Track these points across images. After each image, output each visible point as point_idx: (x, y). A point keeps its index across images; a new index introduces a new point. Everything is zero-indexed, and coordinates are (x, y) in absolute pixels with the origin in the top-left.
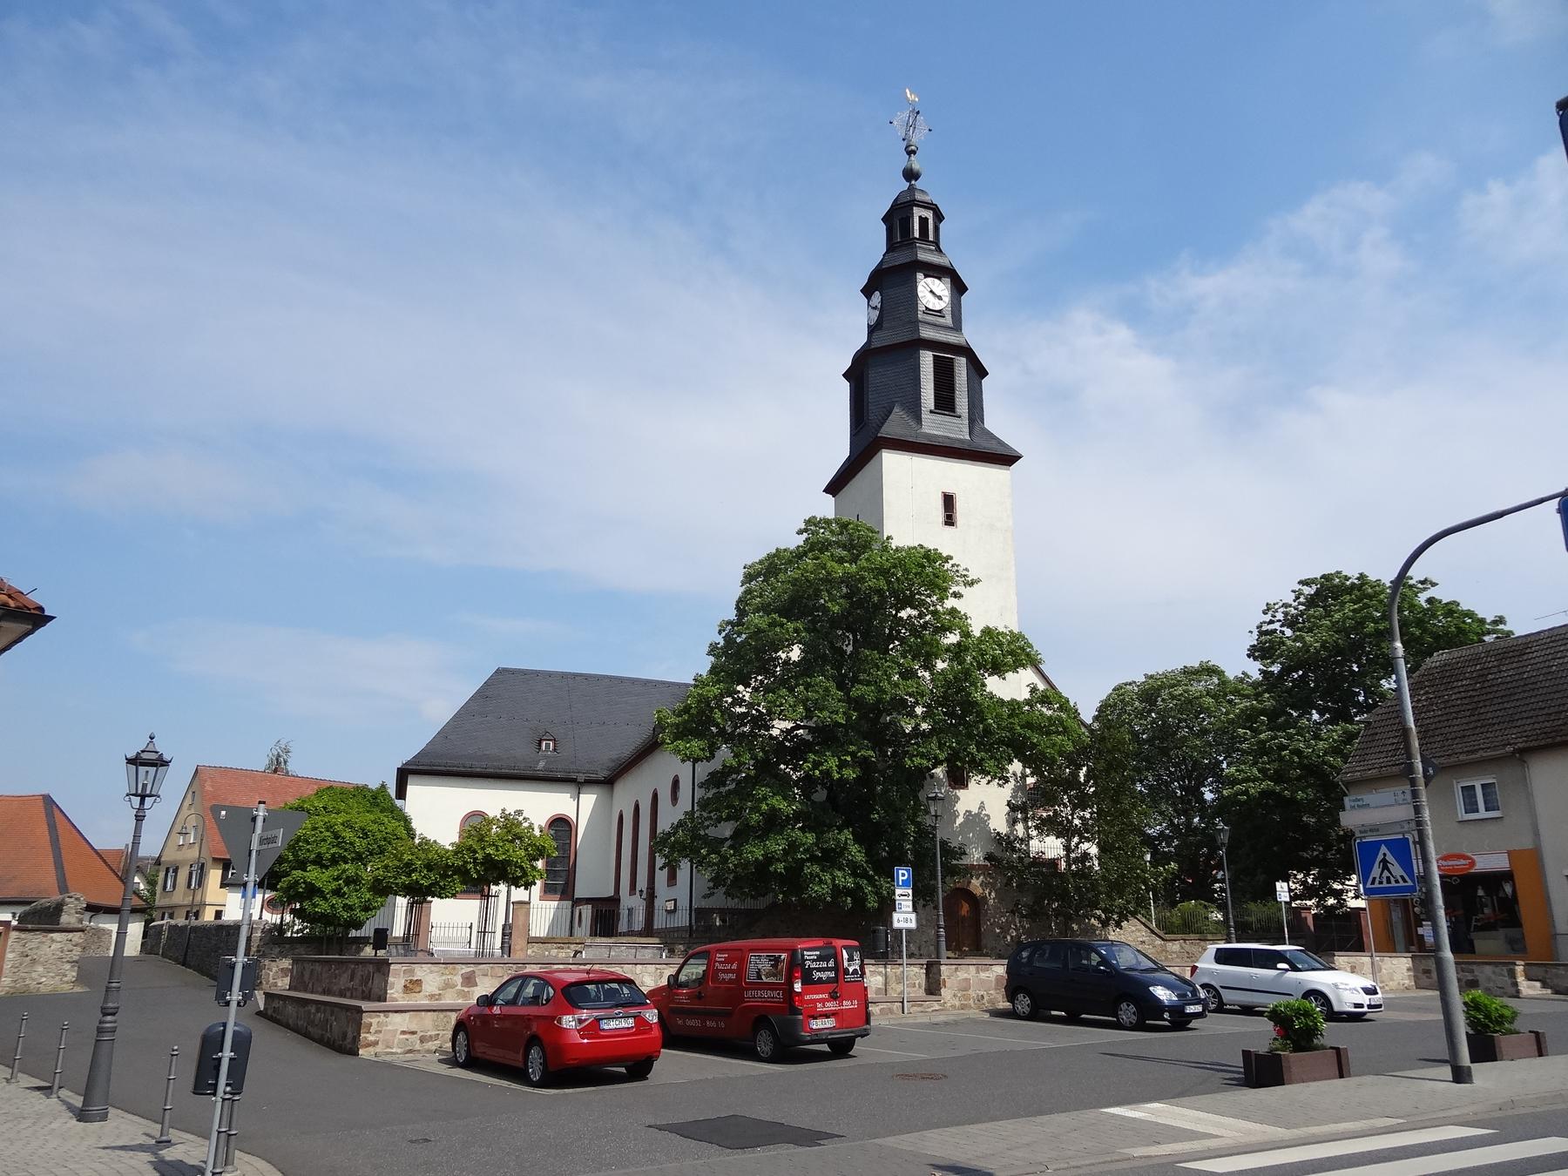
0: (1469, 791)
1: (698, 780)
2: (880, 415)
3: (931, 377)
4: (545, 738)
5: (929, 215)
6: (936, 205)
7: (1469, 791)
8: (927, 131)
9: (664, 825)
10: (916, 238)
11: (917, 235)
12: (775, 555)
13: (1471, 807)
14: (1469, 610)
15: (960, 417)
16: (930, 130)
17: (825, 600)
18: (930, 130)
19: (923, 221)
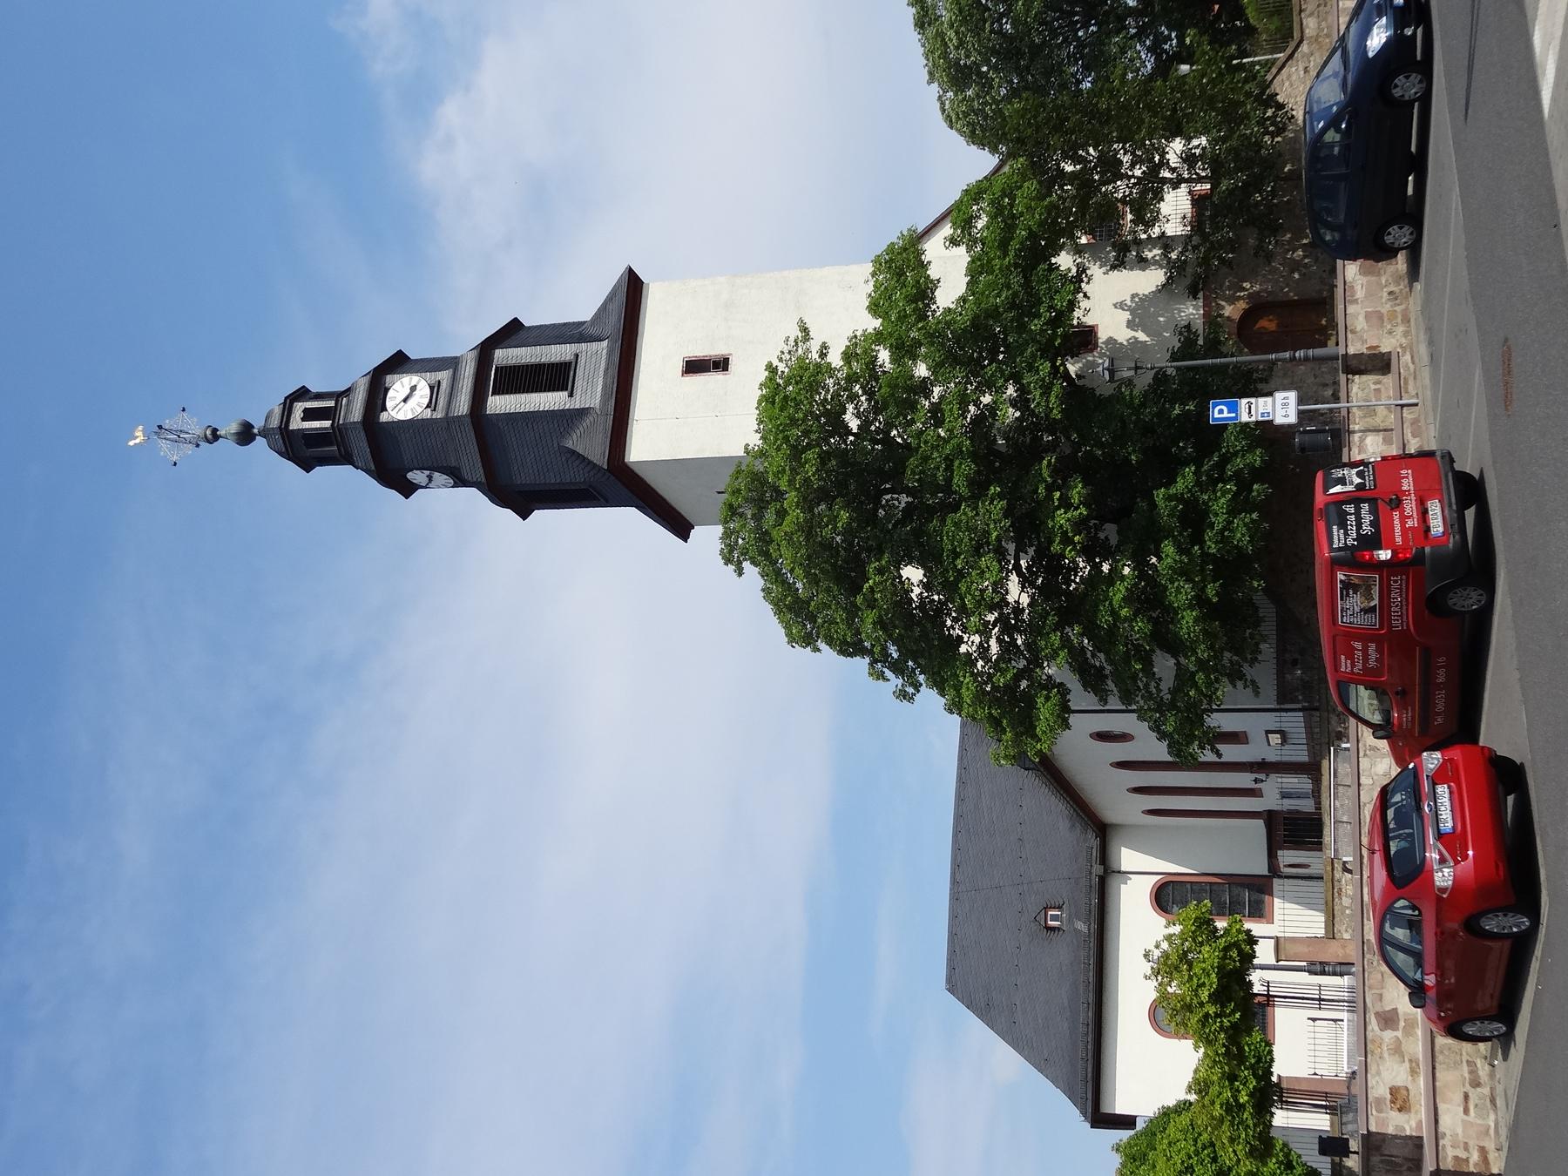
5: (299, 407)
8: (185, 414)
10: (332, 424)
11: (327, 424)
15: (577, 356)
16: (184, 410)
18: (184, 410)
19: (309, 415)
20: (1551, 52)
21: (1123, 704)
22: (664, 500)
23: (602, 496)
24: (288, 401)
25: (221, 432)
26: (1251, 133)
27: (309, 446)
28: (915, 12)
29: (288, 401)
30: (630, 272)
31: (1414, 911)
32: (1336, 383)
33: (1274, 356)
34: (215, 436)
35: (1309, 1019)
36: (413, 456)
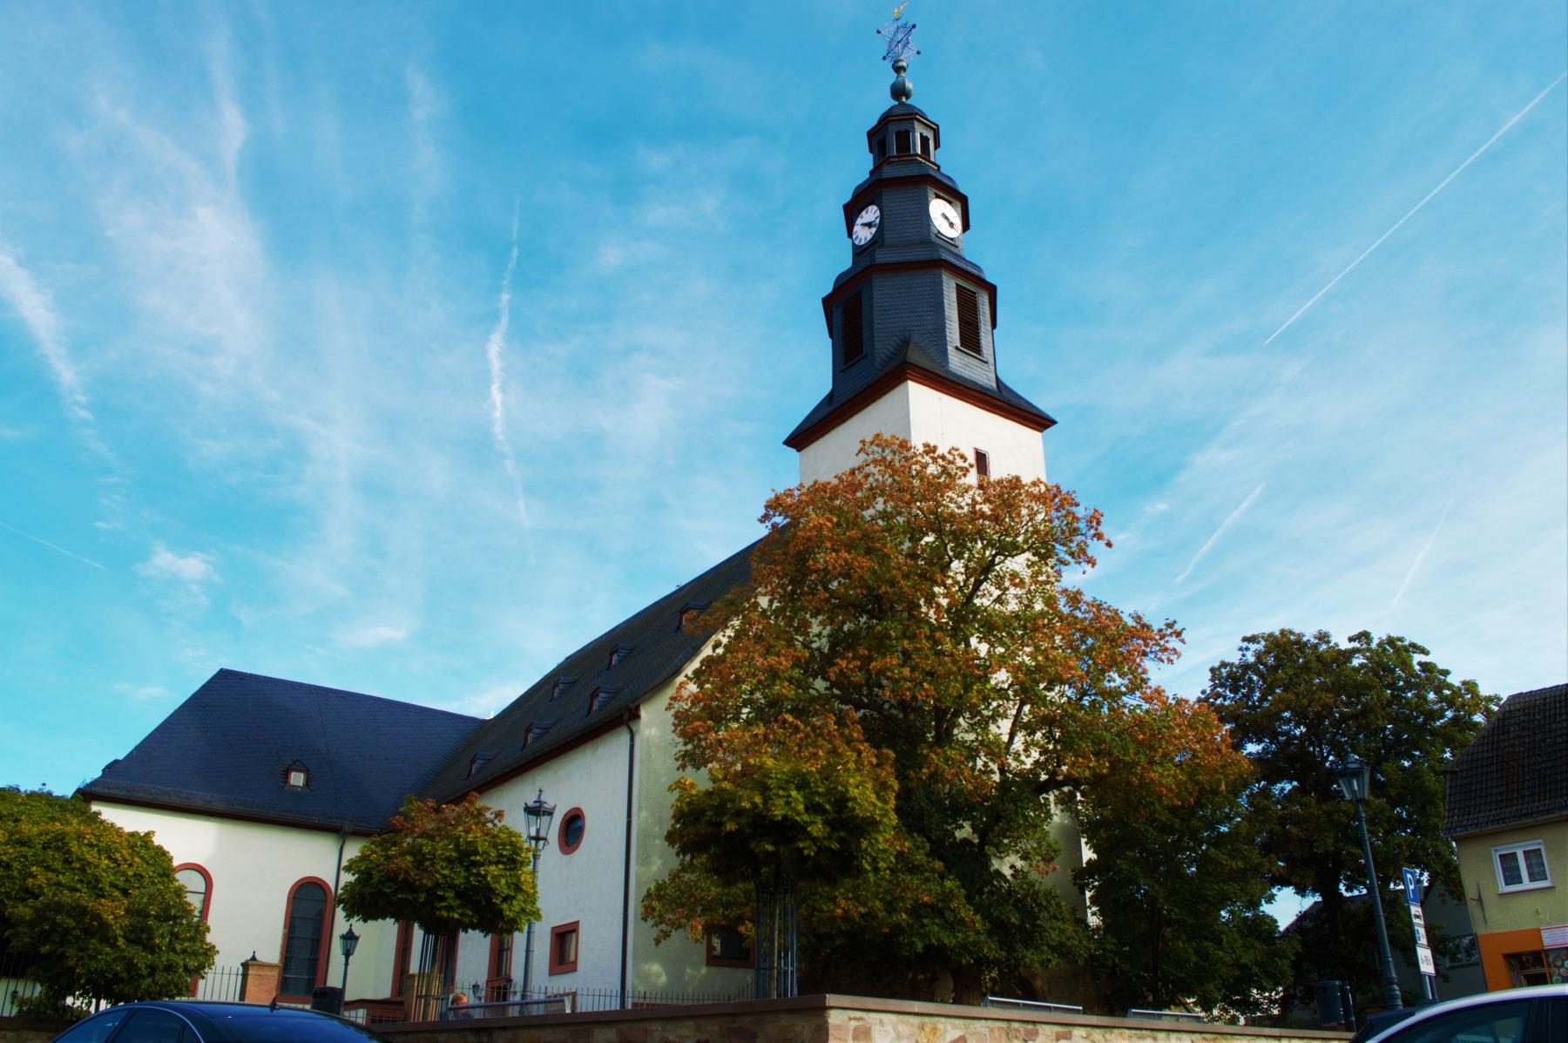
0: (1509, 862)
1: (638, 884)
2: (887, 349)
3: (955, 305)
4: (294, 767)
5: (930, 135)
6: (937, 126)
7: (1509, 862)
8: (915, 52)
9: (916, 124)
10: (918, 155)
11: (919, 151)
12: (201, 967)
13: (1512, 876)
14: (1398, 650)
15: (986, 363)
16: (918, 53)
17: (1053, 766)
18: (918, 53)
19: (924, 140)
20: (630, 990)
21: (346, 886)
22: (844, 421)
23: (847, 368)
24: (935, 127)
25: (903, 74)
26: (682, 917)
27: (898, 134)
28: (1449, 679)
29: (935, 127)
30: (1054, 422)
31: (342, 889)
32: (1349, 1029)
33: (1390, 959)
34: (898, 69)
35: (857, 455)
36: (895, 212)
